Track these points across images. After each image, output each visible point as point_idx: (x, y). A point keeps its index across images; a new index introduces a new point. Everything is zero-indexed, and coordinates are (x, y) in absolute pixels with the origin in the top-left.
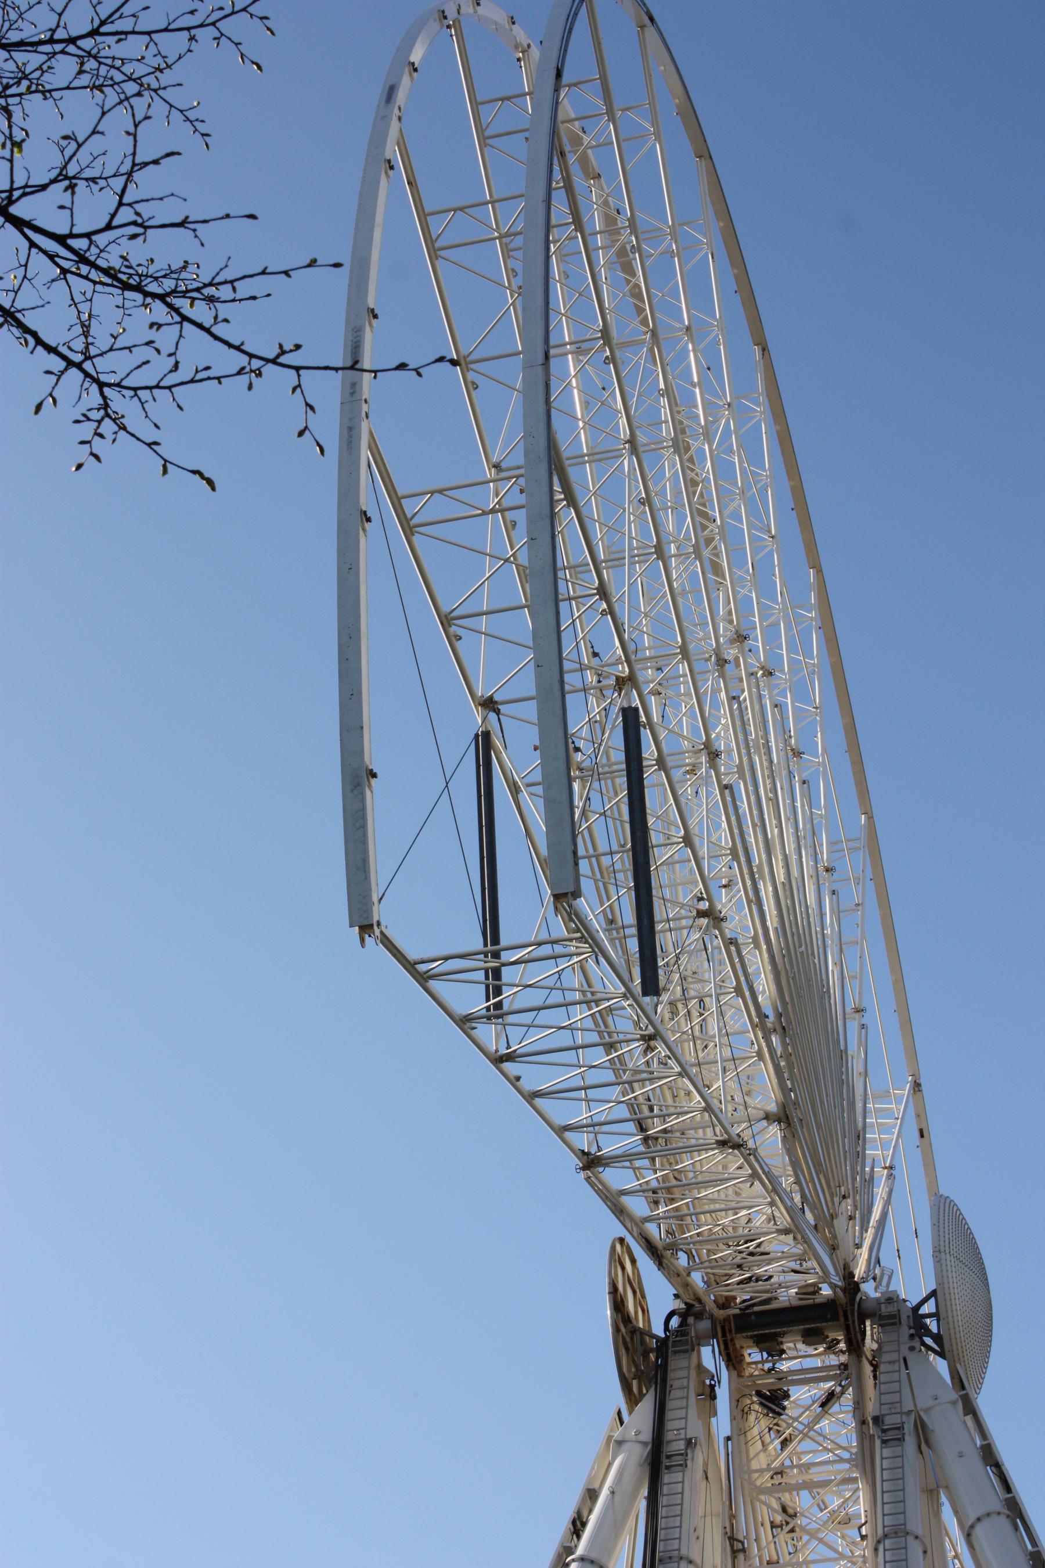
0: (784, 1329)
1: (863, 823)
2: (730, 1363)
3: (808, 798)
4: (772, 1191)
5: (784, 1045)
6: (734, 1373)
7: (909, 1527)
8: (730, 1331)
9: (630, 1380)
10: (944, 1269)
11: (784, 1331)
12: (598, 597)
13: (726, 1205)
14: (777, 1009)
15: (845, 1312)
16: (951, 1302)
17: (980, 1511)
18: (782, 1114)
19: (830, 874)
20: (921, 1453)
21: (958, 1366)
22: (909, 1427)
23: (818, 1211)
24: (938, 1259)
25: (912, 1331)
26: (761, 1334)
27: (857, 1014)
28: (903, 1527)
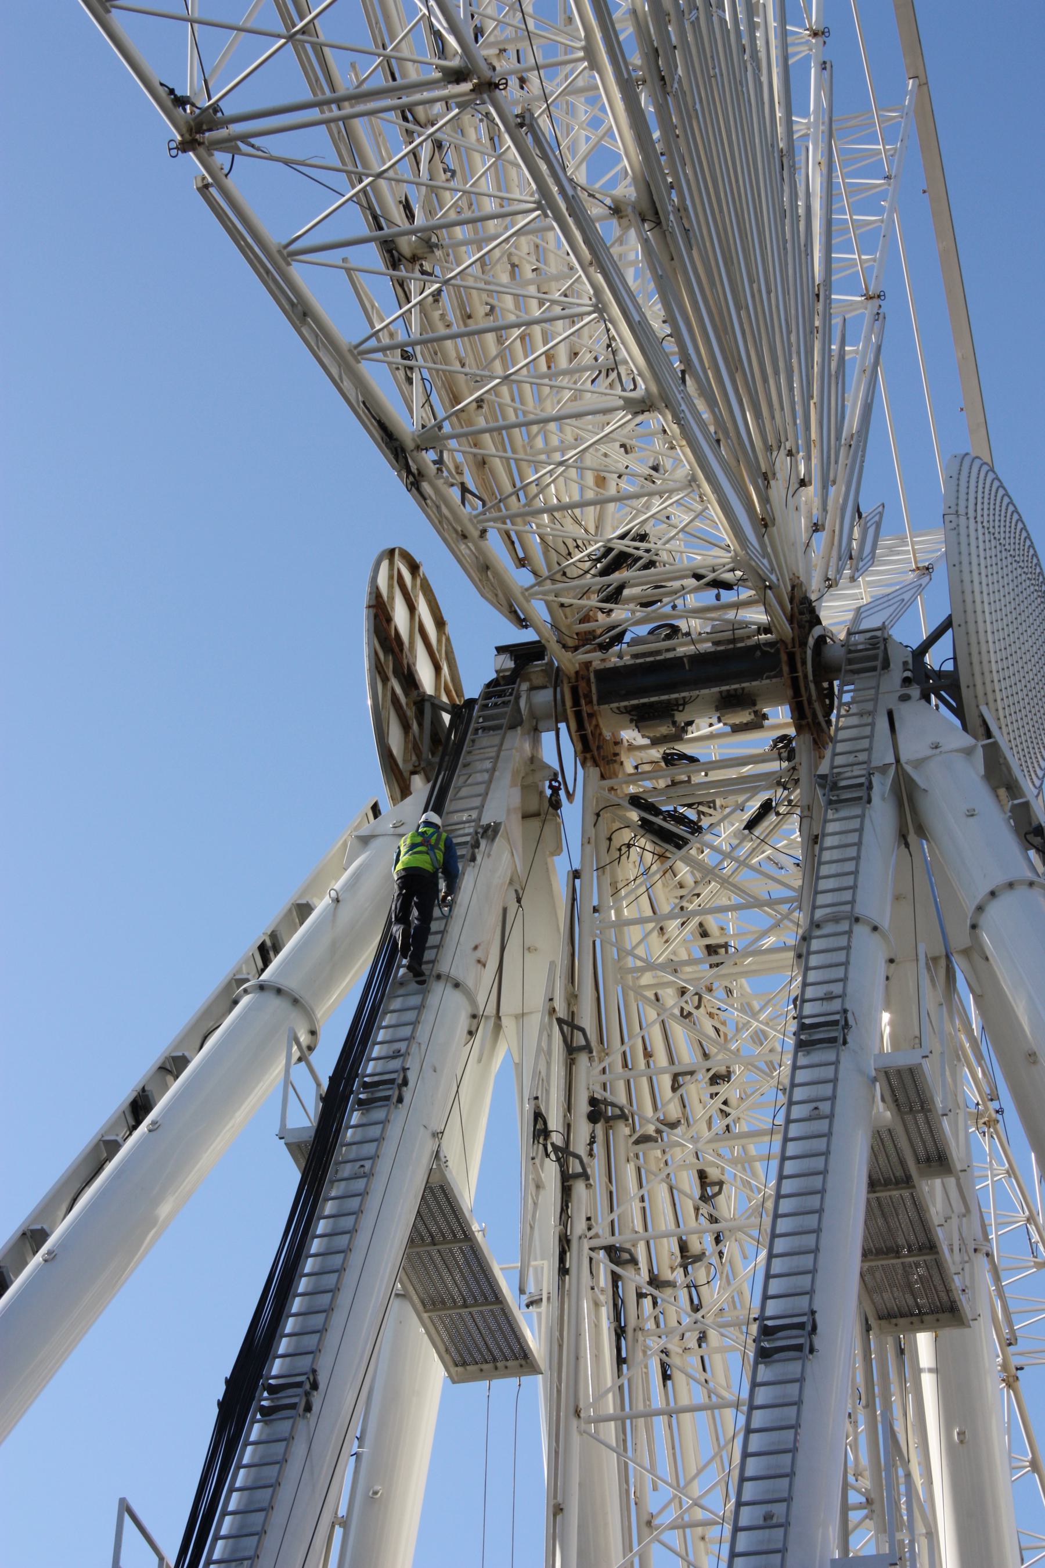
0: (683, 694)
1: (910, 88)
2: (588, 755)
3: (827, 89)
4: (591, 264)
5: (662, 111)
6: (594, 772)
7: (860, 910)
8: (590, 702)
9: (406, 774)
10: (966, 578)
11: (684, 698)
12: (586, 64)
13: (518, 317)
14: (652, 41)
15: (791, 657)
16: (977, 627)
17: (999, 879)
18: (645, 205)
19: (821, 39)
20: (907, 845)
21: (984, 709)
22: (882, 787)
23: (732, 441)
24: (953, 525)
25: (908, 674)
26: (644, 704)
27: (870, 301)
28: (848, 908)
